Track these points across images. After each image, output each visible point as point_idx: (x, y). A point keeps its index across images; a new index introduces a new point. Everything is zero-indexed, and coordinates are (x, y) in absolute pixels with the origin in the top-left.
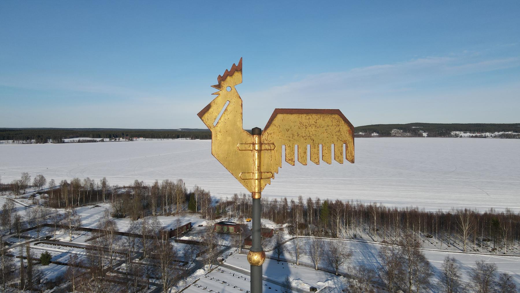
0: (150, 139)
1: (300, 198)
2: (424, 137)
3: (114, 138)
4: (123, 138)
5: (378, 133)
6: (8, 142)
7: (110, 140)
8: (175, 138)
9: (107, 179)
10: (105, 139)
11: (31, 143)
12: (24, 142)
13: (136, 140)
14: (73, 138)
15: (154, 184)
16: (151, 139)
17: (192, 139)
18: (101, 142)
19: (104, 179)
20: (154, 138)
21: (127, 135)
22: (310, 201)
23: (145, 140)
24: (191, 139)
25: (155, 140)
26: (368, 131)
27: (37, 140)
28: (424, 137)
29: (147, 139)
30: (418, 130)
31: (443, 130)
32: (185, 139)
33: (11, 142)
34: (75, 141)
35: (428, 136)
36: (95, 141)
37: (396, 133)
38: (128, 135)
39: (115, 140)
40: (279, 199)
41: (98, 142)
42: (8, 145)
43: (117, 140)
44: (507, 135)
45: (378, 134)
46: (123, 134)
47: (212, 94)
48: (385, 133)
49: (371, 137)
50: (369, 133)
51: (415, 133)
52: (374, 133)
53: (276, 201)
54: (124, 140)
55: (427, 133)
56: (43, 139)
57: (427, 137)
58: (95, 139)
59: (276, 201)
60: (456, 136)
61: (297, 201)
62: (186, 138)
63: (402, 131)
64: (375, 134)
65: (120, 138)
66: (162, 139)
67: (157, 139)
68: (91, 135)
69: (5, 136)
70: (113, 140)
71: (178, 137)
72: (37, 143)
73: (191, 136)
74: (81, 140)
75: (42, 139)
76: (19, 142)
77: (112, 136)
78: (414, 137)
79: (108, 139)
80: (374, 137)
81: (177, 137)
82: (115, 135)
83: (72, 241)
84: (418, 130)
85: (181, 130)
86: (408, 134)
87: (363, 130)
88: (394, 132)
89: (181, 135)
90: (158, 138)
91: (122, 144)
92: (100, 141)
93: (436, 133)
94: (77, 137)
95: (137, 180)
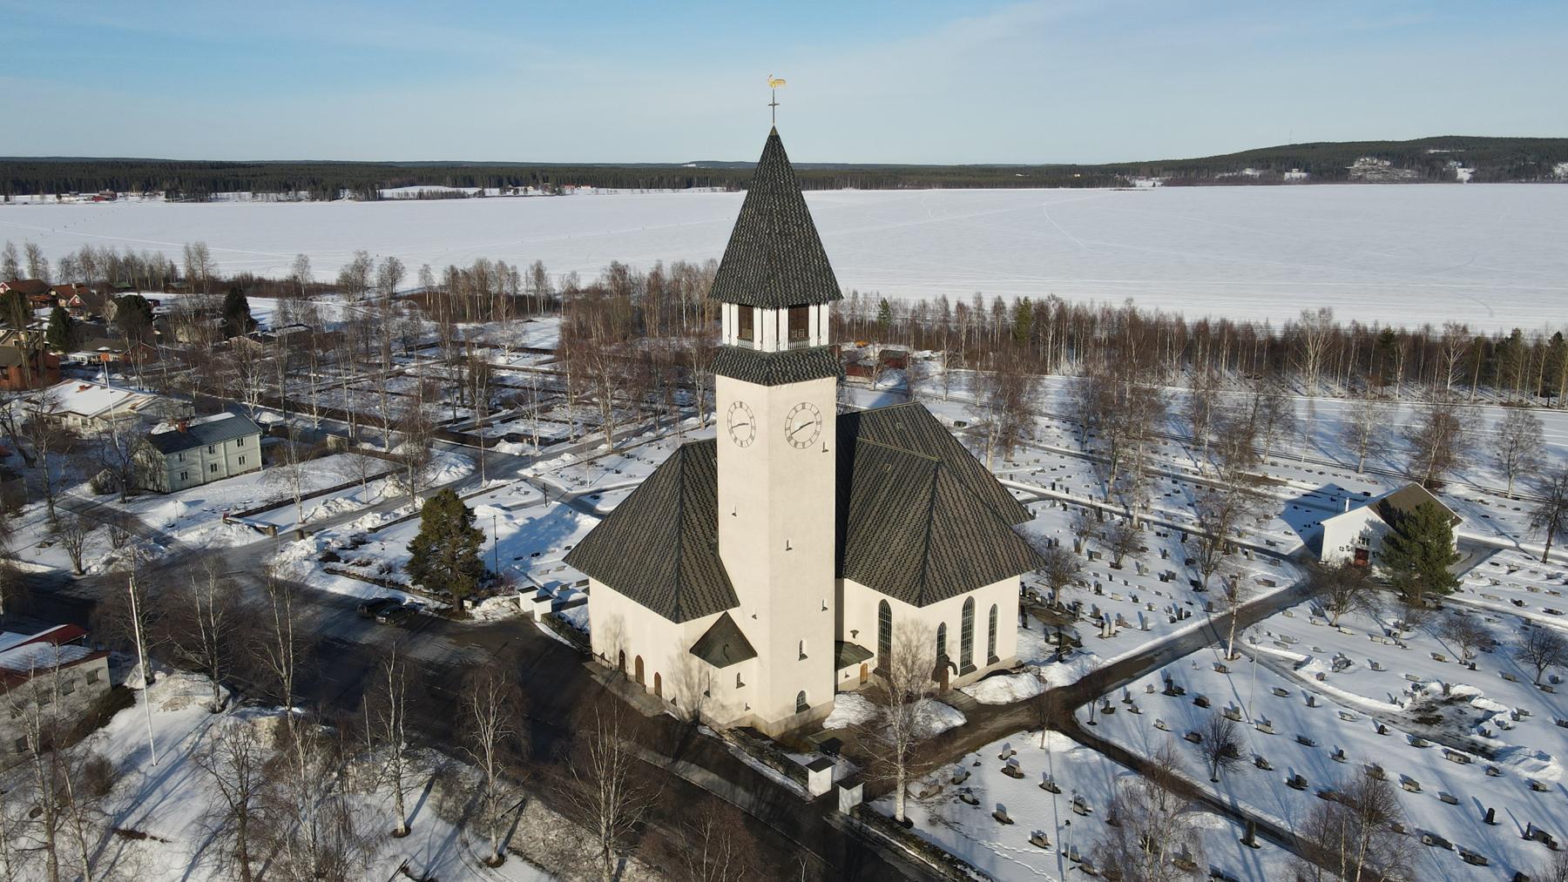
1: (979, 299)
2: (1461, 181)
4: (536, 188)
5: (1305, 171)
6: (240, 197)
10: (487, 191)
11: (300, 200)
12: (282, 196)
13: (573, 193)
14: (401, 186)
21: (546, 180)
23: (597, 193)
25: (624, 194)
26: (1273, 165)
27: (312, 191)
28: (1461, 181)
29: (602, 190)
30: (1443, 159)
31: (1529, 158)
32: (708, 189)
33: (247, 197)
34: (411, 196)
35: (1475, 179)
36: (463, 196)
37: (1365, 170)
40: (930, 301)
41: (469, 197)
42: (241, 204)
43: (521, 193)
44: (1234, 177)
45: (1304, 175)
48: (1327, 172)
49: (1281, 182)
50: (1275, 173)
51: (1433, 168)
52: (1294, 170)
53: (924, 306)
54: (540, 192)
55: (1471, 170)
56: (329, 189)
57: (1468, 182)
58: (462, 190)
60: (217, 199)
61: (969, 302)
63: (1387, 163)
64: (1296, 174)
66: (645, 190)
68: (448, 179)
69: (229, 182)
71: (689, 185)
72: (313, 199)
74: (425, 191)
75: (325, 190)
76: (268, 197)
77: (505, 181)
78: (1424, 181)
79: (496, 191)
80: (1290, 182)
82: (513, 181)
84: (1443, 159)
86: (1408, 173)
87: (1259, 161)
88: (1363, 167)
89: (698, 178)
91: (535, 202)
92: (475, 195)
93: (1501, 169)
94: (412, 184)
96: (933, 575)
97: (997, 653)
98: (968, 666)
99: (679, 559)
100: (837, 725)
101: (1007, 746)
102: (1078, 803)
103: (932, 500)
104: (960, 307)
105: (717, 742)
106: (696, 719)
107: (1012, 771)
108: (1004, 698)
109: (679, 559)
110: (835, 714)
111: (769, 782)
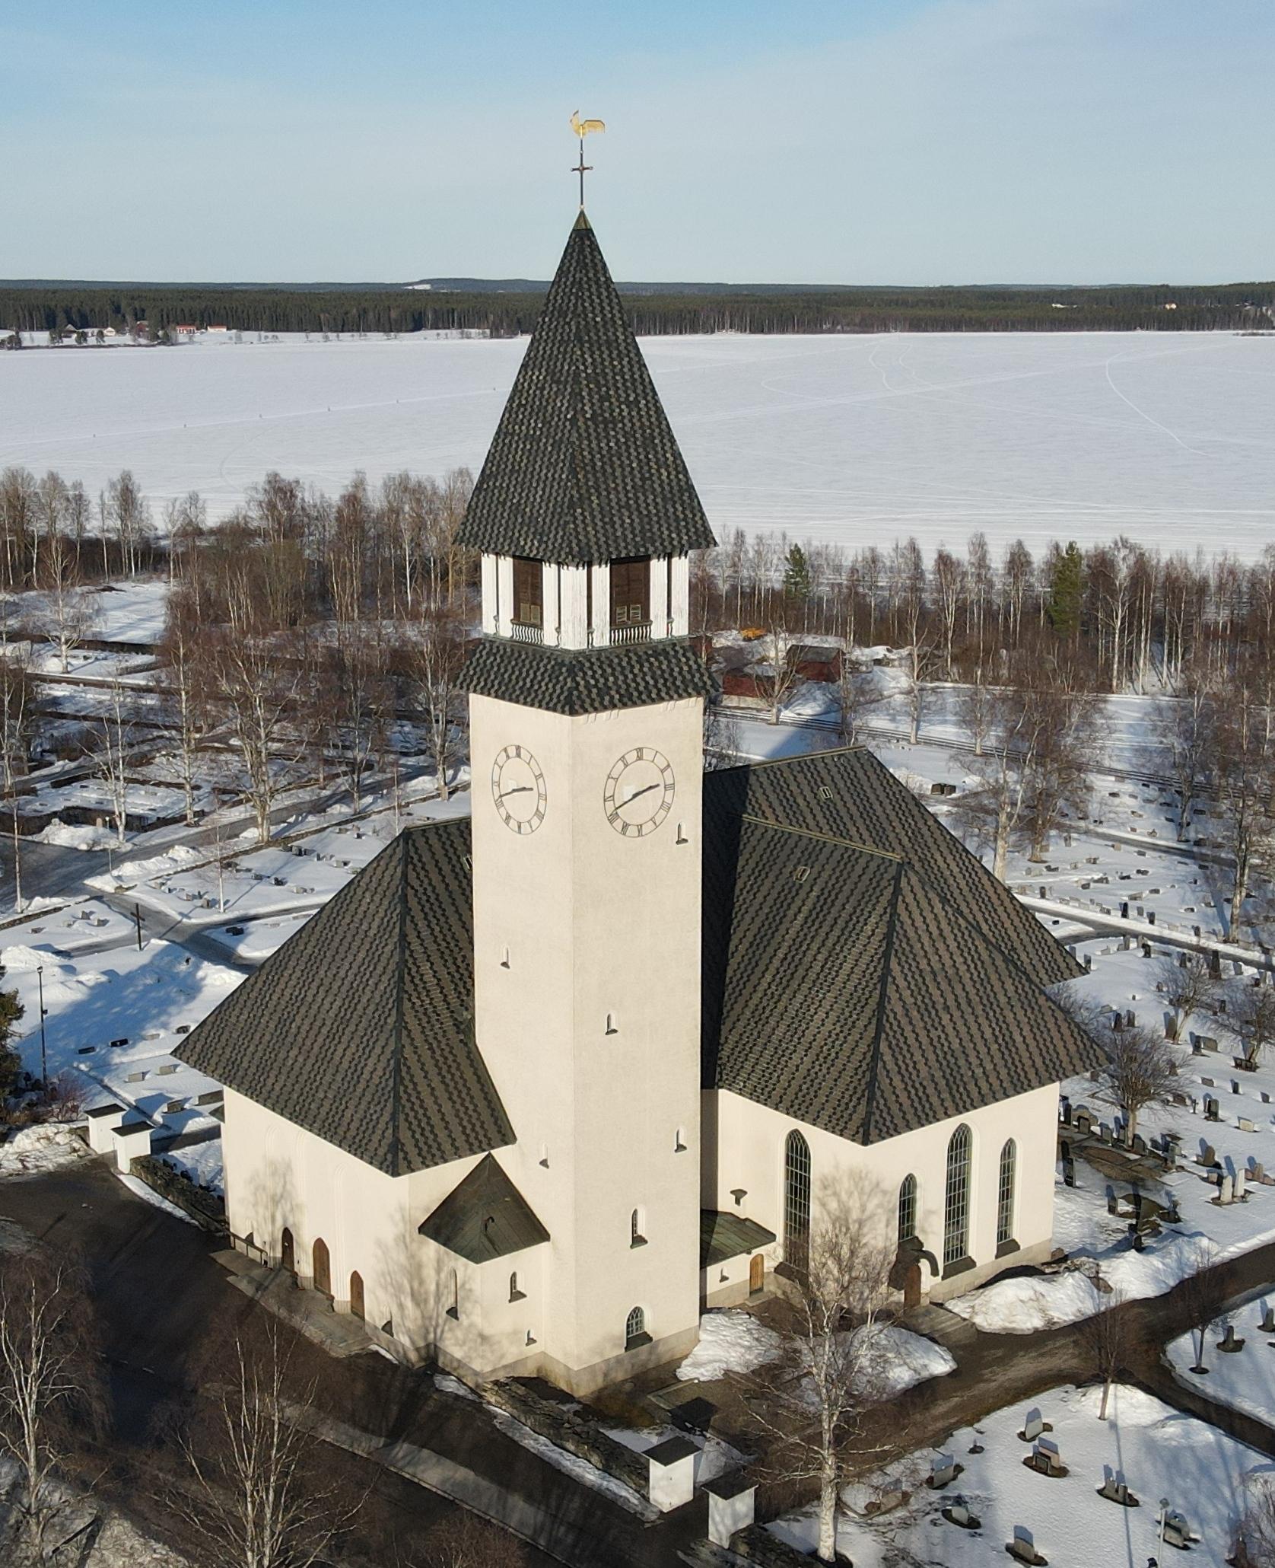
0: (263, 334)
1: (980, 547)
3: (70, 327)
4: (120, 331)
7: (56, 342)
8: (399, 331)
9: (136, 479)
10: (26, 336)
13: (191, 342)
15: (350, 489)
16: (270, 334)
17: (495, 334)
18: (10, 349)
19: (126, 478)
20: (288, 331)
21: (139, 315)
22: (1018, 562)
23: (239, 340)
24: (492, 337)
25: (292, 342)
29: (248, 335)
32: (455, 332)
38: (147, 314)
39: (78, 340)
43: (92, 341)
46: (117, 310)
47: (514, 1275)
54: (128, 338)
59: (874, 560)
61: (960, 552)
62: (460, 328)
65: (105, 332)
66: (332, 335)
67: (303, 334)
70: (72, 340)
73: (491, 317)
77: (61, 317)
79: (43, 337)
81: (411, 327)
82: (75, 317)
83: (68, 672)
85: (427, 287)
89: (435, 311)
90: (305, 331)
95: (276, 475)
96: (892, 1081)
97: (1016, 1233)
98: (958, 1260)
99: (398, 1052)
100: (705, 1374)
101: (1034, 1415)
102: (1174, 1527)
103: (888, 937)
104: (944, 561)
105: (472, 1407)
106: (432, 1362)
107: (1043, 1463)
108: (1029, 1322)
109: (398, 1052)
110: (700, 1352)
111: (571, 1484)
